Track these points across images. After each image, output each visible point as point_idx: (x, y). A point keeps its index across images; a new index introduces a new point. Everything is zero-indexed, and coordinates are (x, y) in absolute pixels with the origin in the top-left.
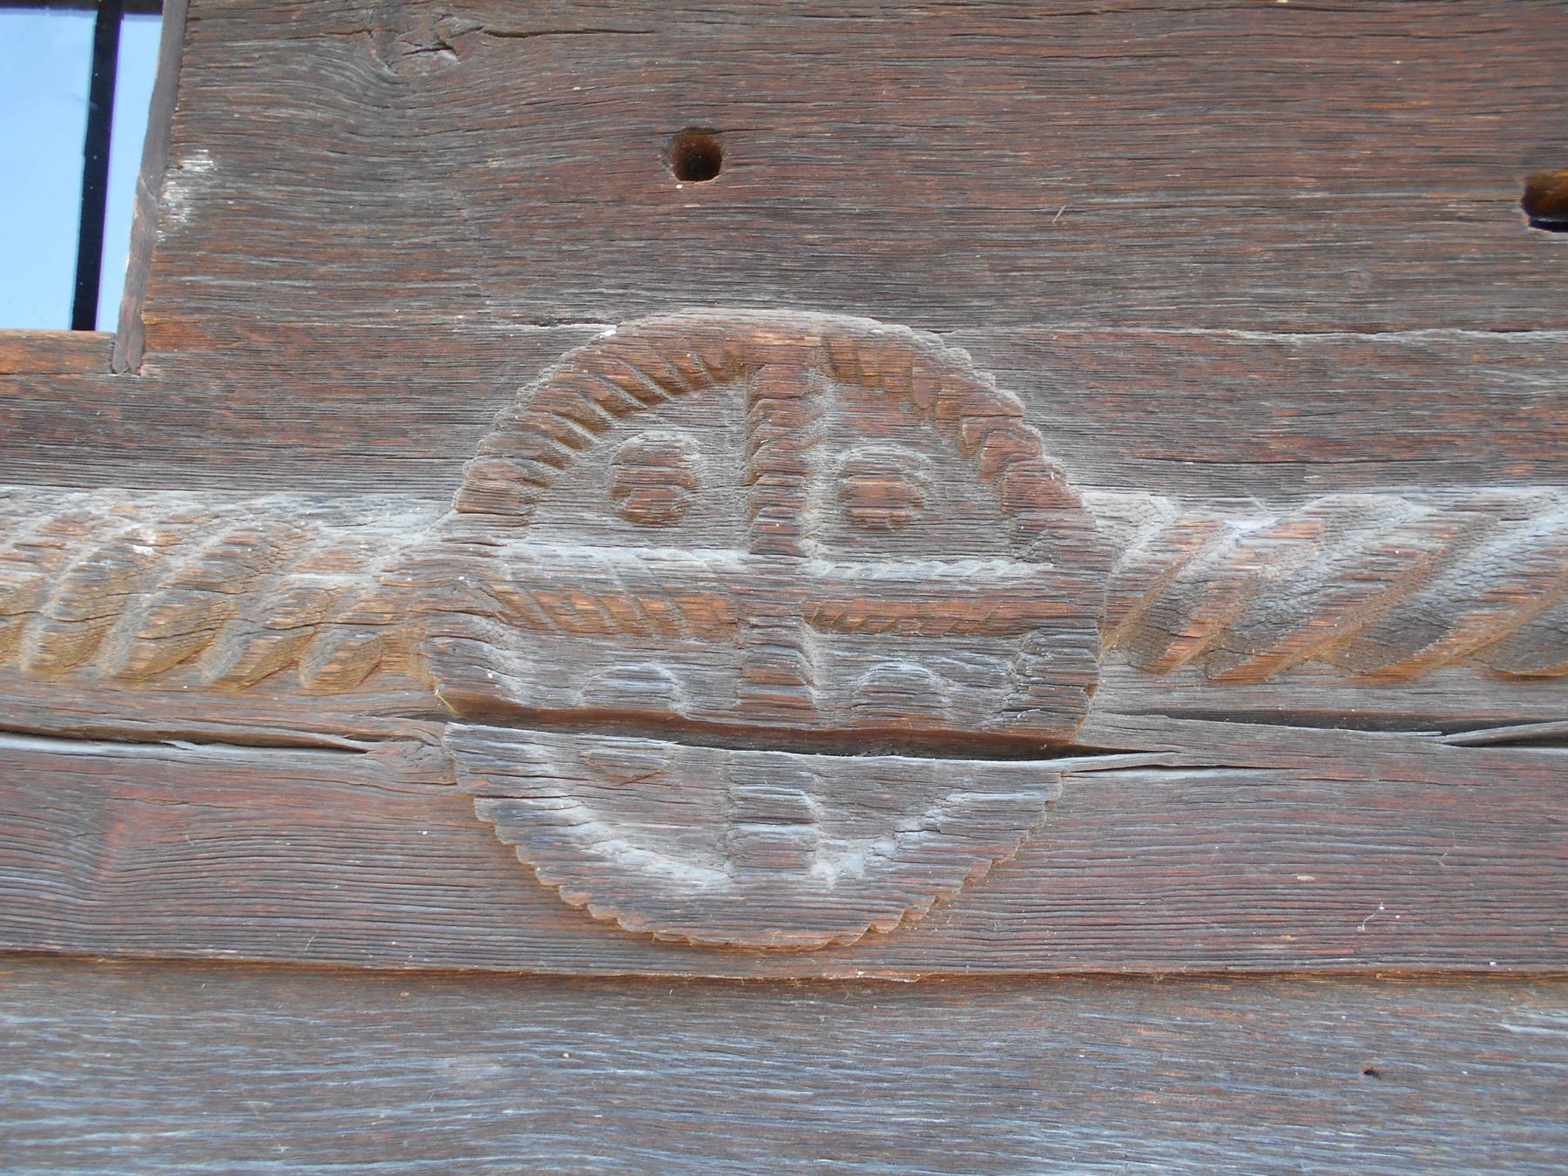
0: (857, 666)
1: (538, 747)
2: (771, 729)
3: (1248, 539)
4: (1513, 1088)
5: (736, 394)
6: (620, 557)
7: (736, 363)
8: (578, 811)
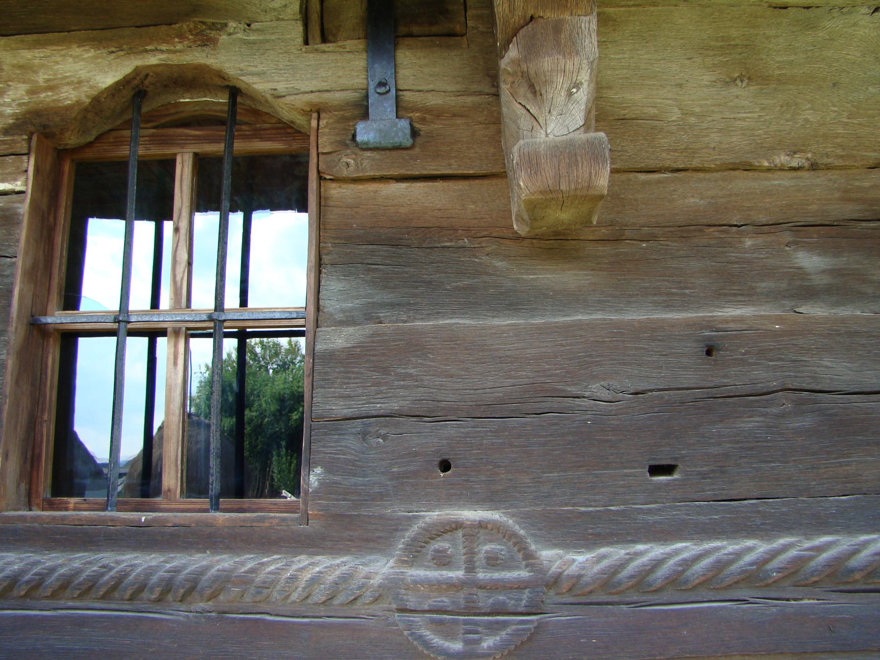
0: (489, 597)
1: (417, 618)
2: (471, 610)
3: (579, 561)
4: (293, 350)
5: (460, 533)
7: (457, 526)
8: (428, 633)
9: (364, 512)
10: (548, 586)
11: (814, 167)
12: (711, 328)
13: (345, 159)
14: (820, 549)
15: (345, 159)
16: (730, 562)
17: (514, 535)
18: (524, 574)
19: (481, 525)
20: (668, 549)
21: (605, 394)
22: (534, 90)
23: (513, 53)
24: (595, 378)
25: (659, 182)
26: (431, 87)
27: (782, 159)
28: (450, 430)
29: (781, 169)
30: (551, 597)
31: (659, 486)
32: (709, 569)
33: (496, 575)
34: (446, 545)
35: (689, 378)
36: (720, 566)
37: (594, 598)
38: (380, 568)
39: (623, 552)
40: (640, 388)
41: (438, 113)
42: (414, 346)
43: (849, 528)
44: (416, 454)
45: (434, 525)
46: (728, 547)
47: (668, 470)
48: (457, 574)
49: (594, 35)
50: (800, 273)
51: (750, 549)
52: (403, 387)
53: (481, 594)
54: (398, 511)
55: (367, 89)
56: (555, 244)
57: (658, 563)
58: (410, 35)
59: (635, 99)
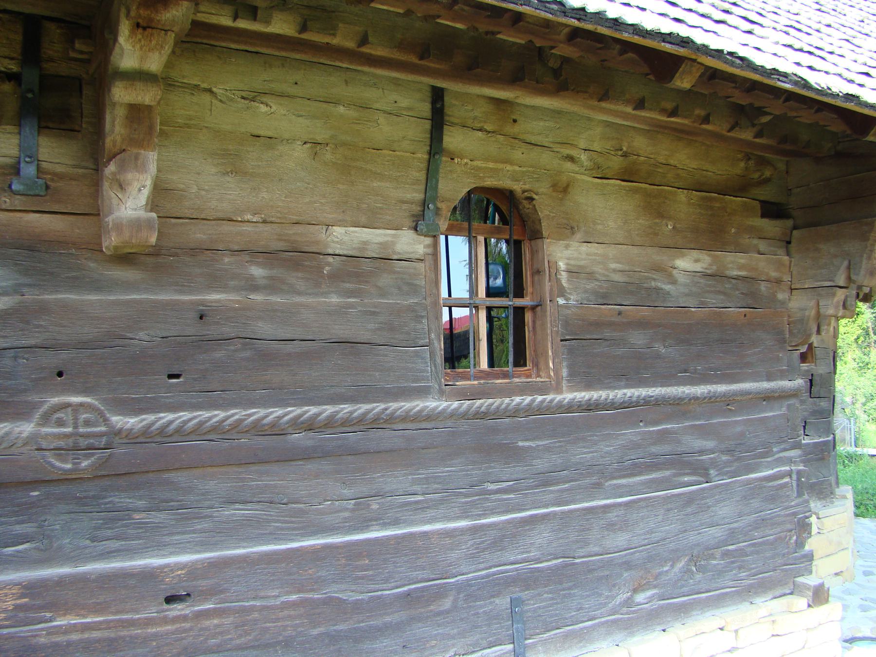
1: (47, 453)
2: (76, 448)
3: (132, 422)
5: (70, 409)
6: (56, 430)
7: (68, 405)
9: (15, 399)
10: (116, 434)
11: (264, 222)
12: (203, 305)
13: (4, 199)
14: (250, 415)
15: (4, 199)
16: (206, 422)
17: (99, 409)
18: (103, 429)
19: (81, 405)
20: (176, 415)
21: (147, 338)
22: (121, 187)
23: (112, 168)
24: (142, 329)
25: (182, 224)
26: (58, 161)
27: (249, 217)
28: (64, 355)
29: (248, 221)
30: (117, 440)
31: (172, 384)
32: (195, 425)
33: (89, 430)
34: (63, 415)
35: (190, 331)
36: (201, 424)
37: (138, 440)
38: (27, 428)
39: (153, 417)
40: (164, 335)
41: (61, 177)
42: (43, 309)
43: (265, 405)
44: (45, 368)
45: (56, 405)
46: (205, 414)
47: (177, 376)
48: (69, 430)
49: (155, 163)
50: (252, 278)
51: (216, 416)
52: (39, 332)
53: (81, 439)
54: (36, 398)
55: (19, 158)
56: (125, 258)
57: (171, 422)
58: (47, 127)
59: (175, 179)
